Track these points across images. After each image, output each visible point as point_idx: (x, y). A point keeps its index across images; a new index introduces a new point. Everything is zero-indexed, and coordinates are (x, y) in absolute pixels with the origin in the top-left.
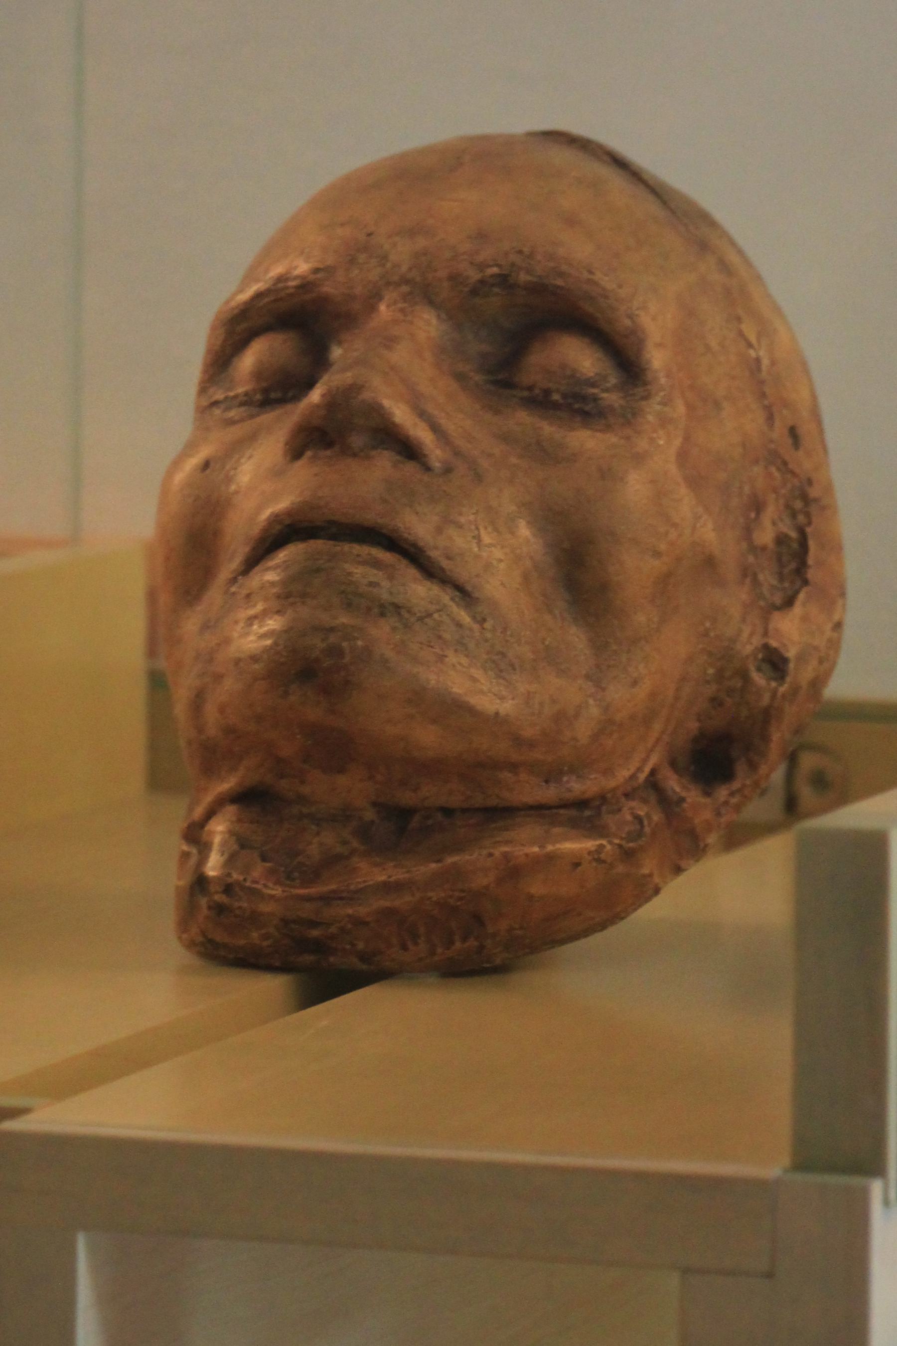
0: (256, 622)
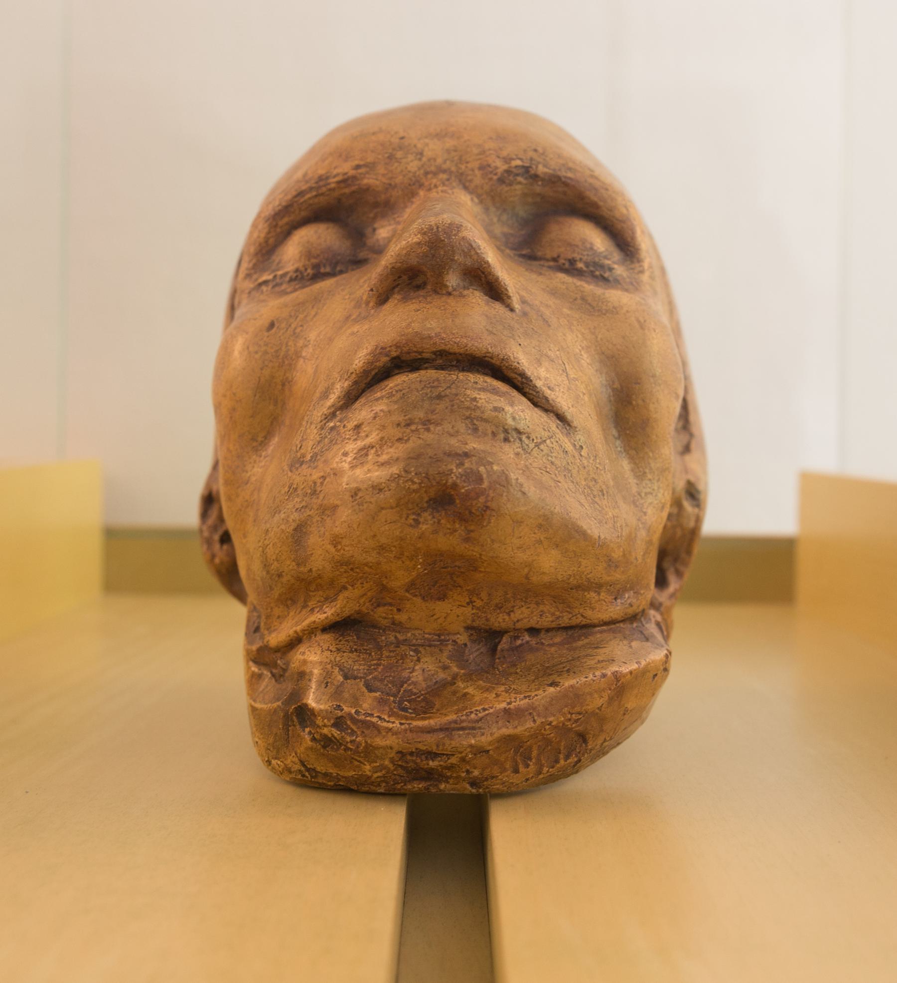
0: (373, 451)
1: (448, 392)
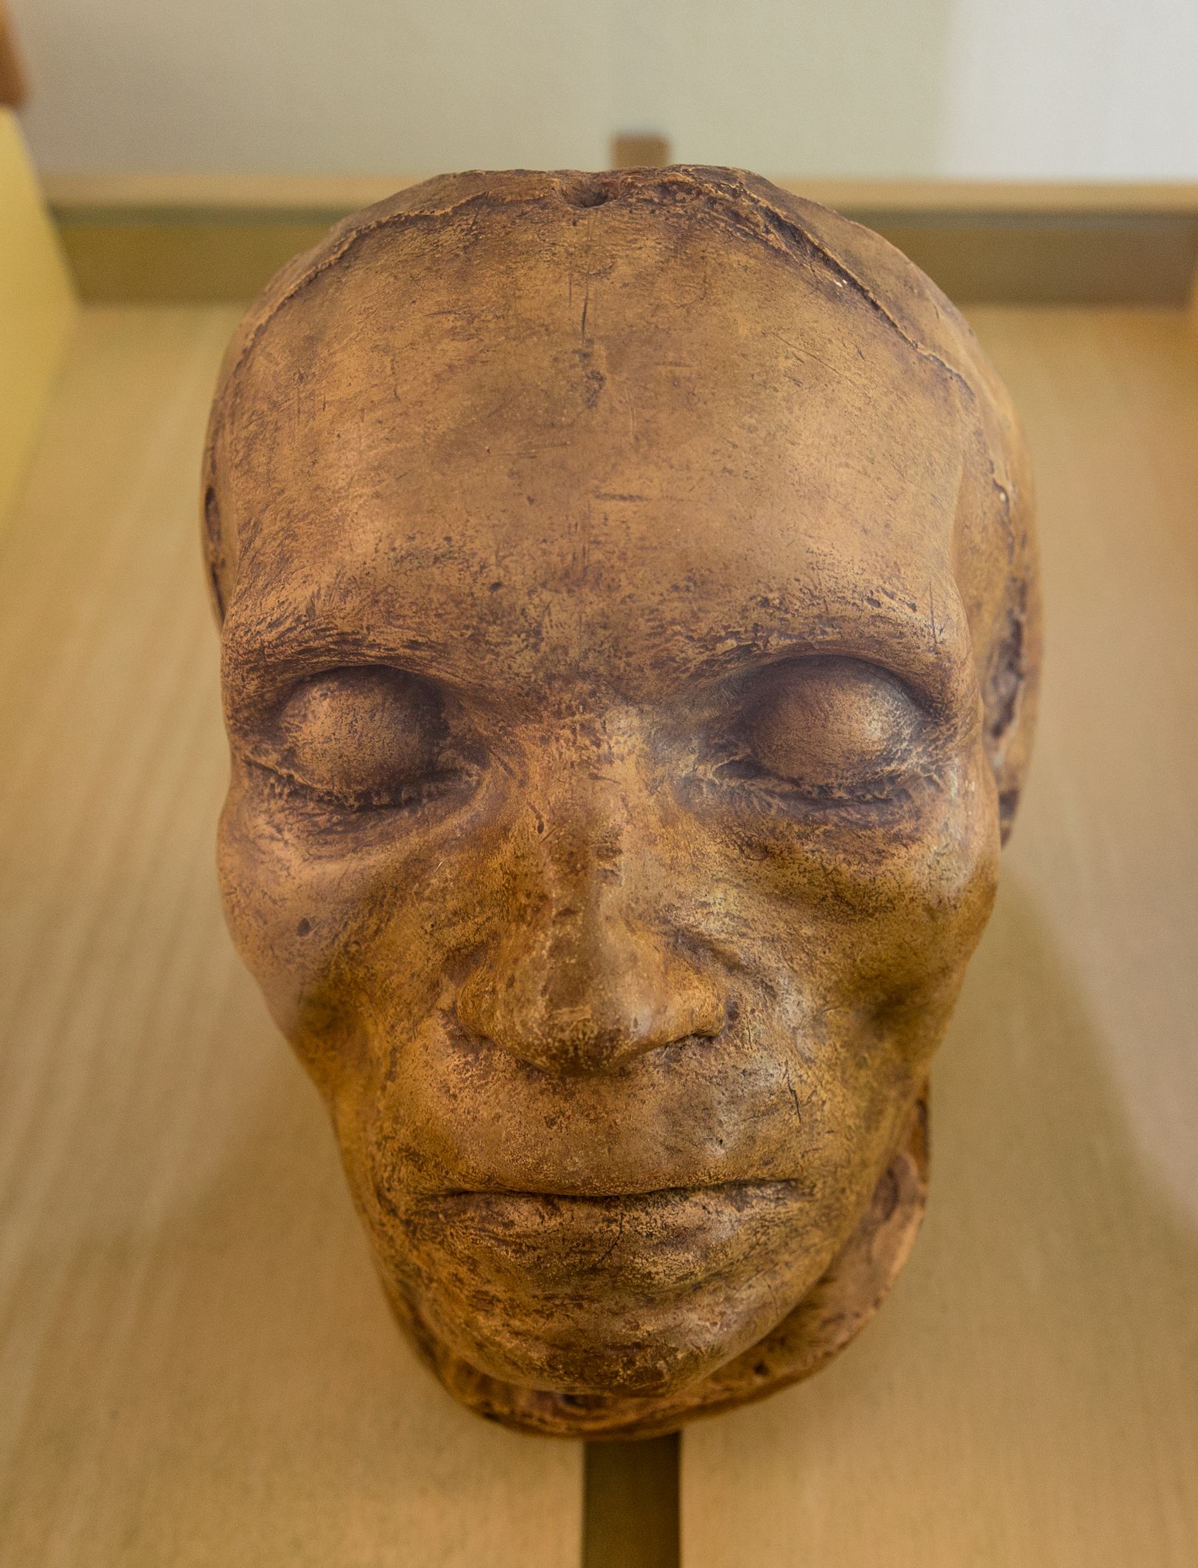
1: (607, 1262)
